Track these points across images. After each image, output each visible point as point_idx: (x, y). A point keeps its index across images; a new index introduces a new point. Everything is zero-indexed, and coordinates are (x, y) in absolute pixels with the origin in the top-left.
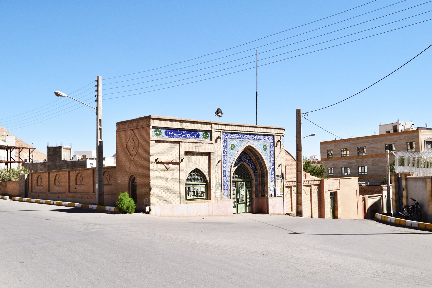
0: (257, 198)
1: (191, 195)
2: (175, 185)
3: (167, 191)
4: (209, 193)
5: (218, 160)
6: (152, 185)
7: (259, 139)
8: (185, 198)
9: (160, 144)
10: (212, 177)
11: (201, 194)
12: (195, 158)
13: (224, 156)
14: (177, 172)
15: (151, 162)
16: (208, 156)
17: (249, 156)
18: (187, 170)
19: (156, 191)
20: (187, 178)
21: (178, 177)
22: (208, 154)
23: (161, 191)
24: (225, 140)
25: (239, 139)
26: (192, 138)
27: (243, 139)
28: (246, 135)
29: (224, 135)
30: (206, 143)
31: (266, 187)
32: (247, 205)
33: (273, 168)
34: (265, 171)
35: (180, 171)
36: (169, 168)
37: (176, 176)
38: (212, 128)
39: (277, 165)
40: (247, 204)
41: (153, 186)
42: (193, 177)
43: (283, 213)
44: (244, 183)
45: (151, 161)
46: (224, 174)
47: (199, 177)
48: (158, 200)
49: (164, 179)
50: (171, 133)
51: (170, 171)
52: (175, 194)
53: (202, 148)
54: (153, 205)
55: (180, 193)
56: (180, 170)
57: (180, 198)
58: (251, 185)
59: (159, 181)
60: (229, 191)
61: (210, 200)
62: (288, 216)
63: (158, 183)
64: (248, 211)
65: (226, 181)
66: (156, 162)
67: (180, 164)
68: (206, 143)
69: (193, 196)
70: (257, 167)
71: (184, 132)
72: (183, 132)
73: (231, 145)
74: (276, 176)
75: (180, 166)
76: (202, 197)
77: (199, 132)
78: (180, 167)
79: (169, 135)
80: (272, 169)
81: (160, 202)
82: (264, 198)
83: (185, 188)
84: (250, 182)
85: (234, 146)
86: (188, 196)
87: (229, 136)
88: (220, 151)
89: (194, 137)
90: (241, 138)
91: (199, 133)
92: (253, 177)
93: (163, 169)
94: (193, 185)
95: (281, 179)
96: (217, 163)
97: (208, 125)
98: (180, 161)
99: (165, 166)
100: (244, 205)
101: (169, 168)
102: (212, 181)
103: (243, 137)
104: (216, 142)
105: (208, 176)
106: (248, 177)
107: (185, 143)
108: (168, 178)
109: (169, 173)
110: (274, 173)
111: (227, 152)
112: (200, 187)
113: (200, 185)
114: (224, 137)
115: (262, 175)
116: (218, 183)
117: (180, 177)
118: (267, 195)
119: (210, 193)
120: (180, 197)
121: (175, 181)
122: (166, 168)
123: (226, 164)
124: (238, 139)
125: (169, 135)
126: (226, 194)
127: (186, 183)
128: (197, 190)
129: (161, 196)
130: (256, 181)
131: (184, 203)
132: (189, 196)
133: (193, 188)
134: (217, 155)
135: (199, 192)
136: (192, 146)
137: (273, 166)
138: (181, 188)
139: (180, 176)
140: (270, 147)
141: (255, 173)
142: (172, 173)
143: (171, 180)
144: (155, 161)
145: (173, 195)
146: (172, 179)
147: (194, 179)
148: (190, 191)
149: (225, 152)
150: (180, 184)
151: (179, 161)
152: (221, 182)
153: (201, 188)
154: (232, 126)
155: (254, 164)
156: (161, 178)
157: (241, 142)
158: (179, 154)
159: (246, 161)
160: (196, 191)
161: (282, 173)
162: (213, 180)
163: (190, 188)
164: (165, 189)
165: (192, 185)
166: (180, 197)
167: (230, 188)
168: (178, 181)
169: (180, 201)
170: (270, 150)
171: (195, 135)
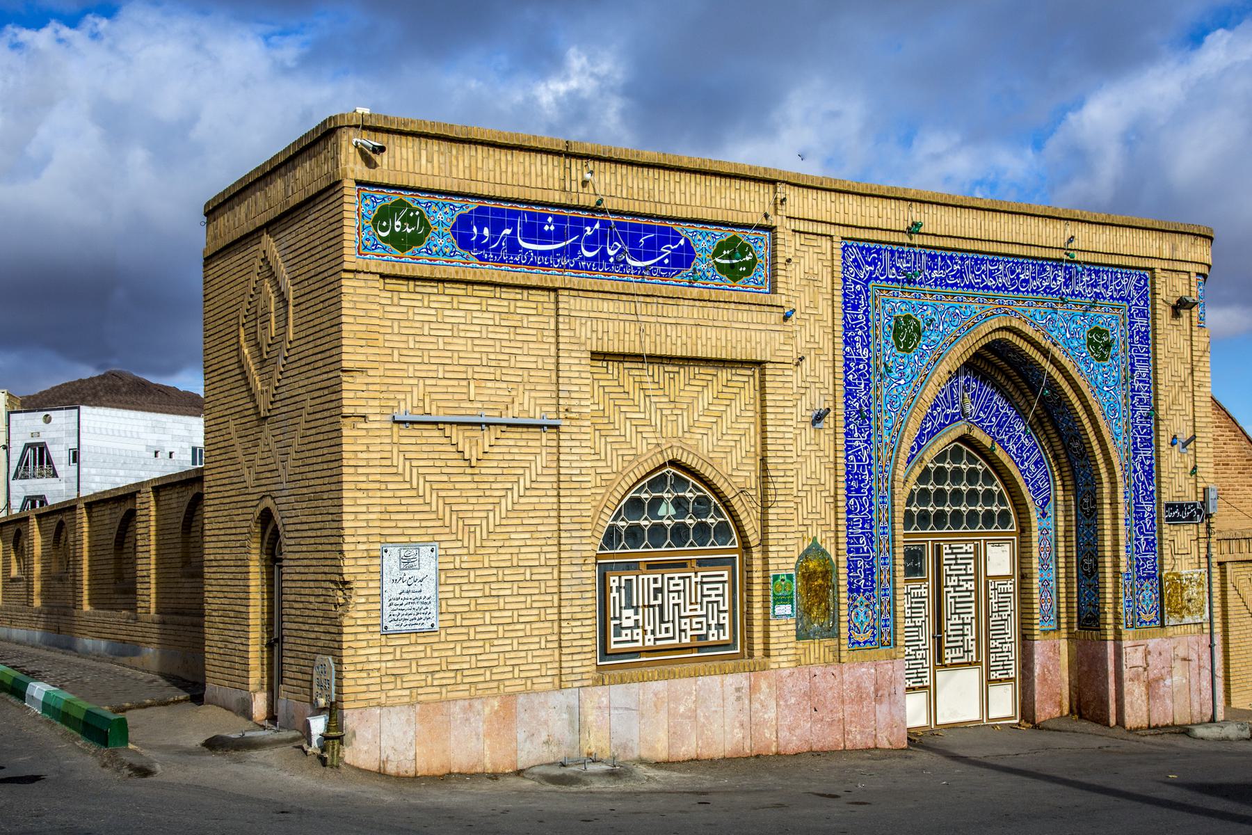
2: (522, 570)
5: (809, 413)
14: (534, 485)
24: (860, 292)
27: (970, 291)
29: (855, 260)
41: (359, 577)
51: (492, 479)
69: (649, 636)
87: (884, 269)
89: (661, 263)
93: (438, 463)
108: (478, 522)
111: (871, 363)
124: (939, 288)
125: (486, 246)
131: (585, 683)
135: (689, 607)
140: (1131, 337)
149: (859, 361)
153: (706, 586)
157: (957, 304)
159: (982, 421)
160: (672, 602)
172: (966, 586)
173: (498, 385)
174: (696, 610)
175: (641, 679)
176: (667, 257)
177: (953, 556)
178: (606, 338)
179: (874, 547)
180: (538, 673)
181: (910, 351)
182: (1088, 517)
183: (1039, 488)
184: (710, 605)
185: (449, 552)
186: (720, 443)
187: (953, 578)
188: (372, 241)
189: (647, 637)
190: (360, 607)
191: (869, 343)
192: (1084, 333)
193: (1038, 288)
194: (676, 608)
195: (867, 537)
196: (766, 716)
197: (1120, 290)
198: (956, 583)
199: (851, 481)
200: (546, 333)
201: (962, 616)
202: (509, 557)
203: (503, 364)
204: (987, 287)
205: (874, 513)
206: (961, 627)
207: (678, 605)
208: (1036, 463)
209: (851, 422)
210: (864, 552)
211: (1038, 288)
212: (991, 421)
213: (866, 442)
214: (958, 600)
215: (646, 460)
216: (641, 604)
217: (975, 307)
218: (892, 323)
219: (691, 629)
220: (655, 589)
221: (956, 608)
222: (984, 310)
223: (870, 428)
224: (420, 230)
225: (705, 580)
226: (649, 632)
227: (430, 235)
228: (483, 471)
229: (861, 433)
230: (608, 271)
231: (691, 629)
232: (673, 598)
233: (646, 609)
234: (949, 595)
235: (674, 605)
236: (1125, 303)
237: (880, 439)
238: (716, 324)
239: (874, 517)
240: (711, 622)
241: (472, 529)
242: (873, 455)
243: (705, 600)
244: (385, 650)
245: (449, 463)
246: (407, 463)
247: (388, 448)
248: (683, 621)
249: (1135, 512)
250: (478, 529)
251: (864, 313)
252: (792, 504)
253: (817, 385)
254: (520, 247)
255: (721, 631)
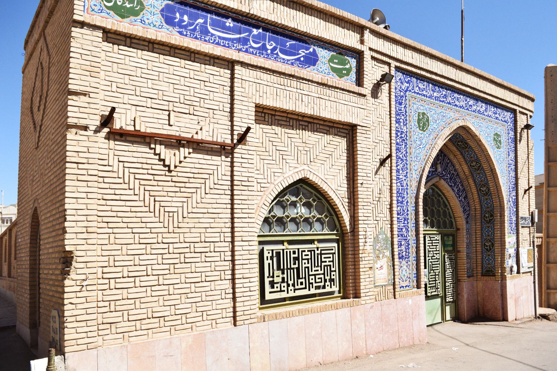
0: (471, 278)
1: (283, 281)
2: (208, 245)
3: (167, 272)
4: (350, 270)
5: (379, 157)
6: (76, 242)
7: (485, 113)
8: (258, 296)
9: (134, 55)
10: (361, 213)
11: (322, 276)
12: (301, 141)
13: (397, 144)
14: (216, 186)
15: (76, 126)
16: (346, 137)
17: (451, 163)
18: (265, 181)
19: (100, 275)
20: (265, 213)
21: (225, 206)
22: (346, 131)
23: (131, 274)
24: (403, 96)
25: (440, 101)
26: (288, 60)
27: (449, 105)
28: (456, 95)
29: (400, 79)
30: (343, 90)
31: (497, 249)
32: (447, 301)
33: (514, 198)
34: (496, 204)
35: (232, 181)
36: (177, 164)
37: (214, 201)
38: (362, 42)
39: (521, 192)
40: (446, 297)
41: (79, 248)
42: (292, 213)
43: (534, 314)
44: (439, 237)
45: (71, 121)
46: (399, 204)
47: (314, 213)
48: (112, 317)
49: (148, 214)
50: (193, 17)
51: (186, 180)
52: (208, 284)
53: (328, 103)
54: (85, 347)
55: (233, 279)
56: (232, 176)
57: (234, 299)
58: (454, 244)
59: (122, 225)
60: (415, 263)
61: (357, 299)
62: (545, 321)
63: (115, 231)
64: (448, 317)
65: (404, 230)
66: (106, 130)
67: (232, 153)
68: (343, 90)
69: (291, 288)
70: (470, 196)
71: (255, 32)
72: (251, 32)
73: (419, 116)
74: (520, 218)
75: (232, 162)
76: (328, 289)
77: (316, 48)
78: (232, 166)
79: (181, 27)
80: (511, 200)
81: (124, 326)
82: (494, 277)
83: (257, 256)
84: (453, 236)
85: (428, 120)
86: (273, 287)
87: (413, 87)
88: (385, 127)
89: (298, 59)
90: (445, 100)
91: (314, 50)
92: (461, 221)
93: (145, 166)
94: (290, 242)
95: (529, 227)
96: (378, 164)
97: (349, 30)
98: (235, 141)
99: (155, 154)
100: (439, 300)
101: (177, 164)
102: (361, 227)
103: (450, 99)
104: (375, 91)
105: (347, 208)
106: (442, 221)
107: (259, 74)
108: (175, 209)
109: (178, 189)
110: (515, 210)
111: (408, 135)
112: (316, 252)
113: (320, 241)
114: (399, 84)
115: (483, 217)
116: (380, 236)
117: (232, 209)
118: (503, 269)
119: (355, 272)
120: (234, 293)
121: (207, 225)
122: (165, 166)
123: (405, 172)
124: (437, 102)
125: (185, 27)
126: (404, 273)
127: (259, 236)
128: (306, 261)
129: (130, 296)
130: (468, 232)
131: (252, 321)
132: (275, 289)
133: (292, 256)
134: (379, 138)
135: (314, 269)
136: (287, 88)
137: (514, 194)
138: (236, 258)
139: (232, 204)
140: (508, 139)
141: (464, 211)
142: (194, 190)
143: (186, 220)
144: (98, 123)
145: (198, 290)
146: (191, 215)
147: (293, 220)
148: (279, 268)
149: (402, 133)
150: (233, 237)
151: (229, 141)
152: (392, 231)
153: (323, 256)
154: (423, 57)
155: (462, 185)
156: (133, 209)
157: (444, 111)
158: (232, 112)
159: (444, 176)
160: (304, 266)
161: (531, 212)
162: (366, 226)
163: (278, 254)
164: (155, 262)
165: (285, 244)
166: (234, 293)
167: (416, 252)
168: (223, 225)
169: (235, 312)
170: (508, 149)
171: (302, 53)
172: (437, 256)
173: (192, 117)
174: (318, 270)
175: (288, 316)
176: (303, 56)
177: (431, 242)
178: (265, 96)
179: (410, 234)
180: (220, 316)
181: (424, 131)
182: (488, 223)
183: (466, 210)
184: (326, 268)
185: (153, 230)
186: (331, 170)
187: (431, 252)
188: (98, 7)
189: (290, 288)
190: (79, 271)
191: (407, 124)
192: (492, 135)
193: (476, 110)
194: (307, 269)
195: (406, 228)
196: (360, 333)
197: (504, 118)
198: (432, 255)
199: (399, 197)
200: (225, 88)
201: (435, 271)
202: (198, 235)
203: (195, 103)
204: (456, 105)
205: (409, 215)
206: (434, 277)
207: (308, 268)
208: (464, 198)
209: (399, 165)
210: (404, 237)
211: (476, 110)
212: (447, 176)
213: (405, 176)
214: (433, 263)
215: (289, 177)
216: (285, 267)
217: (452, 114)
218: (417, 115)
219: (316, 282)
220: (293, 257)
221: (432, 267)
222: (455, 116)
223: (407, 169)
224: (136, 7)
225: (323, 252)
226: (291, 285)
227: (144, 12)
228: (179, 174)
229: (403, 171)
230: (267, 58)
231: (316, 282)
232: (305, 263)
233: (289, 271)
234: (430, 261)
235: (305, 268)
236: (506, 124)
237: (411, 175)
238: (330, 99)
239: (409, 218)
240: (326, 277)
241: (171, 214)
242: (408, 184)
243: (323, 264)
244: (101, 304)
245: (154, 167)
246: (121, 164)
247: (106, 152)
248: (311, 277)
249: (510, 221)
250: (176, 214)
251: (404, 108)
252: (370, 208)
253: (383, 142)
254: (209, 32)
255: (332, 283)
